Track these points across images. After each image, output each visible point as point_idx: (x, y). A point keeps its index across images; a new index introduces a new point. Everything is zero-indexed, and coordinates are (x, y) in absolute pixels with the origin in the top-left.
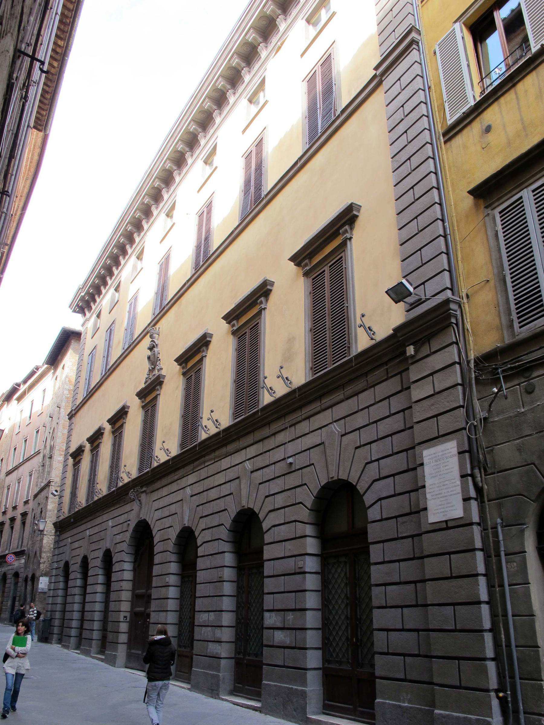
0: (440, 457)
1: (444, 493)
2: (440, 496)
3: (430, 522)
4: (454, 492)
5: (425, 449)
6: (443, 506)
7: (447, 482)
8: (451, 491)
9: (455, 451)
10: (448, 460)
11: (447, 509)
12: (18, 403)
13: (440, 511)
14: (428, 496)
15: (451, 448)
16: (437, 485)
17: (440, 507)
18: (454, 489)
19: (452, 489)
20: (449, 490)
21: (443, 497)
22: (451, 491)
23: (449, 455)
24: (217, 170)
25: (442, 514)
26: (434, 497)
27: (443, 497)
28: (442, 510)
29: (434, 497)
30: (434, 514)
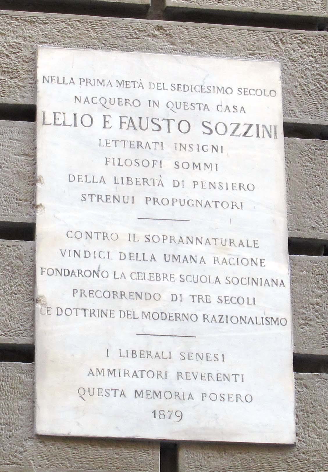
0: (160, 112)
1: (174, 298)
2: (139, 307)
3: (45, 426)
4: (245, 311)
5: (54, 42)
6: (155, 365)
7: (196, 249)
8: (224, 300)
9: (271, 112)
10: (214, 139)
11: (182, 386)
12: (42, 184)
13: (131, 384)
14: (46, 287)
15: (245, 92)
16: (127, 248)
17: (133, 364)
18: (246, 291)
19: (229, 291)
20: (214, 291)
21: (163, 316)
22: (224, 300)
23: (230, 118)
24: (65, 79)
25: (147, 405)
26: (90, 303)
27: (163, 316)
28: (143, 384)
29: (90, 303)
30: (83, 393)
